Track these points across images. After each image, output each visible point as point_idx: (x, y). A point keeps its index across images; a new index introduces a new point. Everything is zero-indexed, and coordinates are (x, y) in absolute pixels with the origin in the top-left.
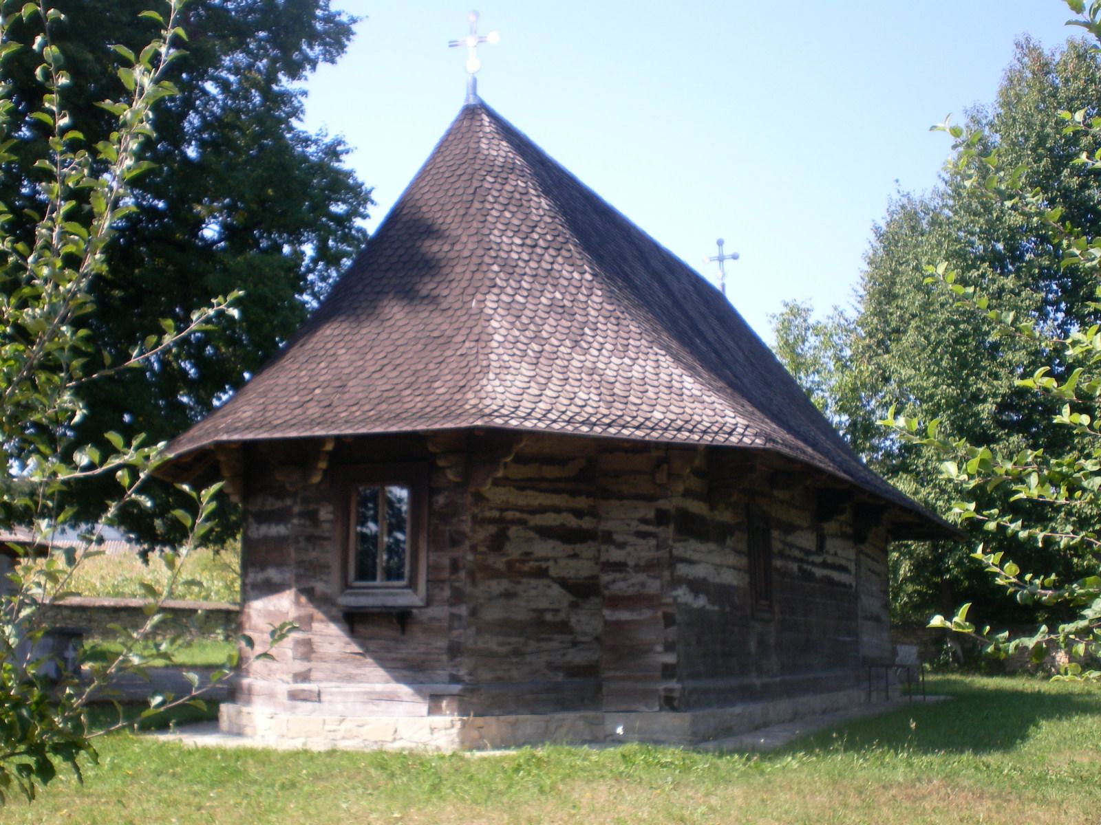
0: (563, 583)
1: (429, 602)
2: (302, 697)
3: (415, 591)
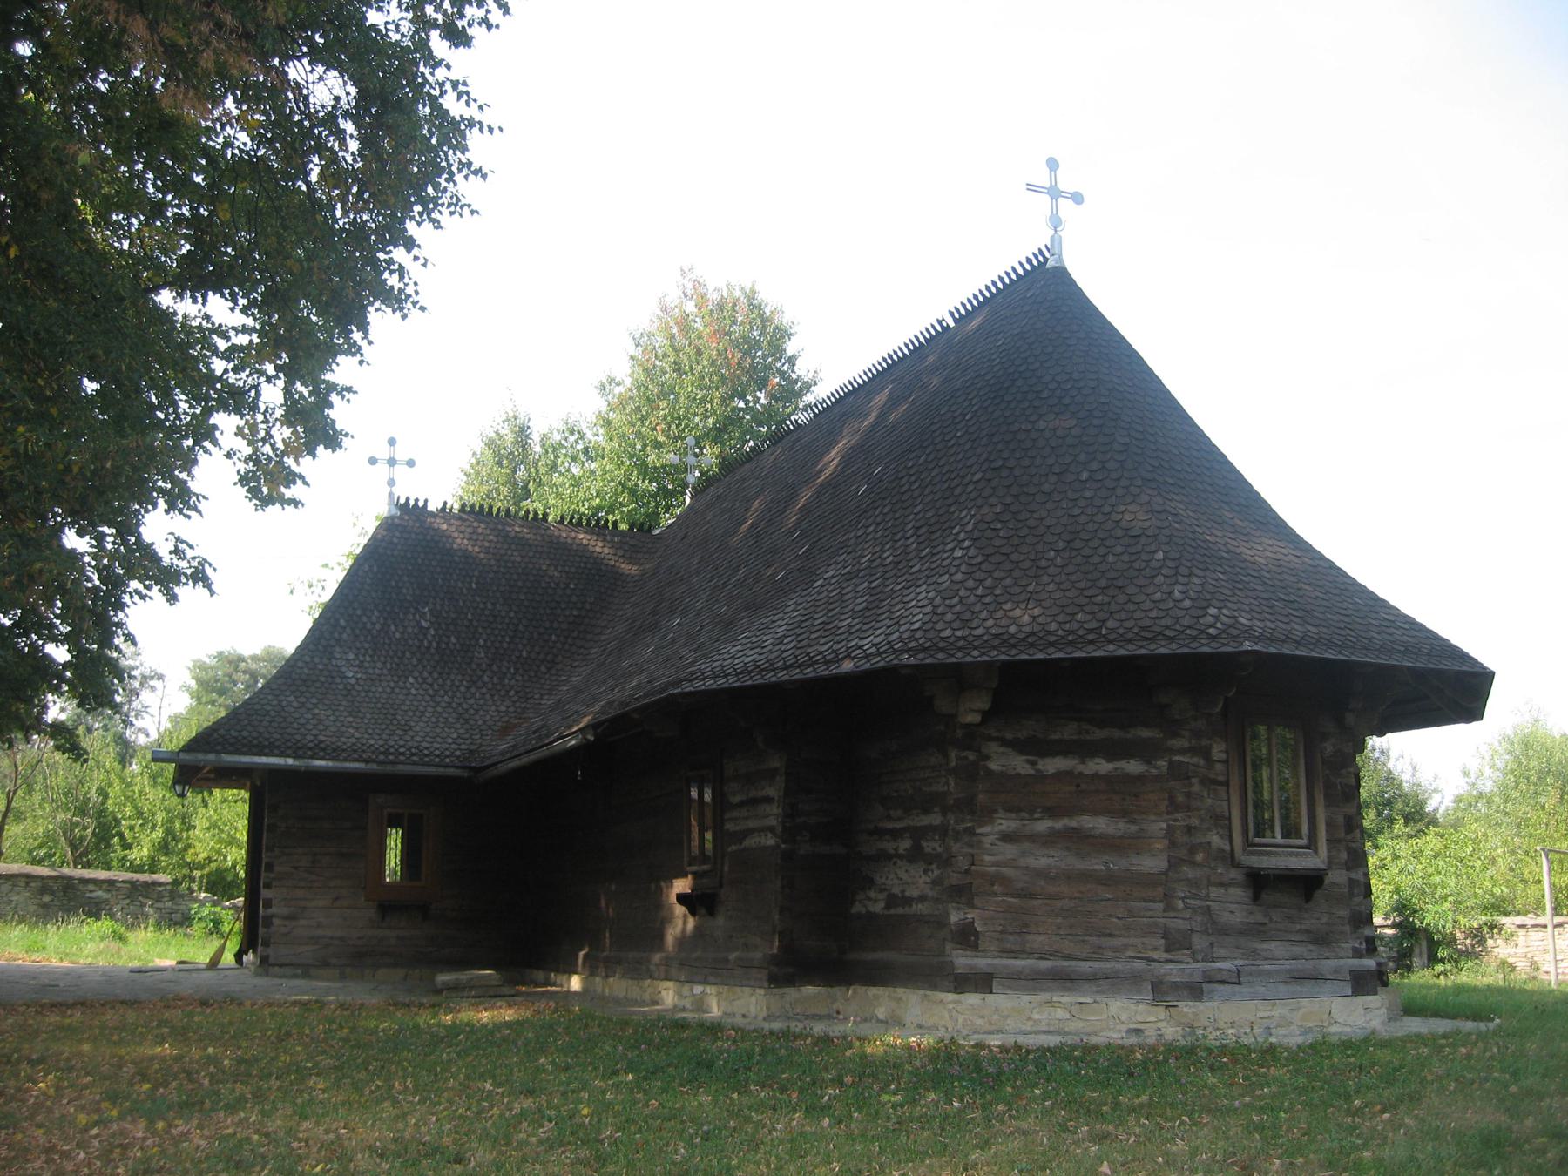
2: (1219, 977)
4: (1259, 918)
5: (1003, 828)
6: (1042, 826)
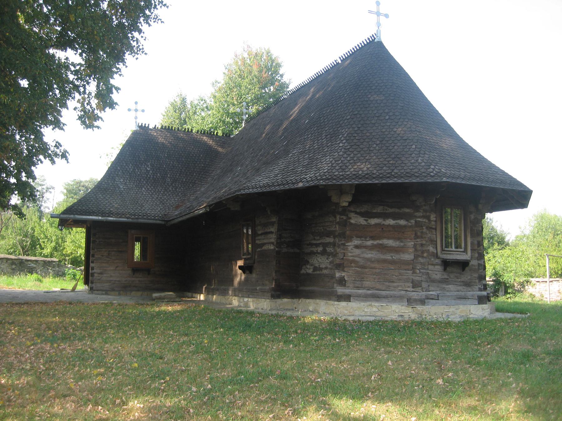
2: (431, 297)
4: (446, 277)
5: (355, 243)
6: (369, 243)
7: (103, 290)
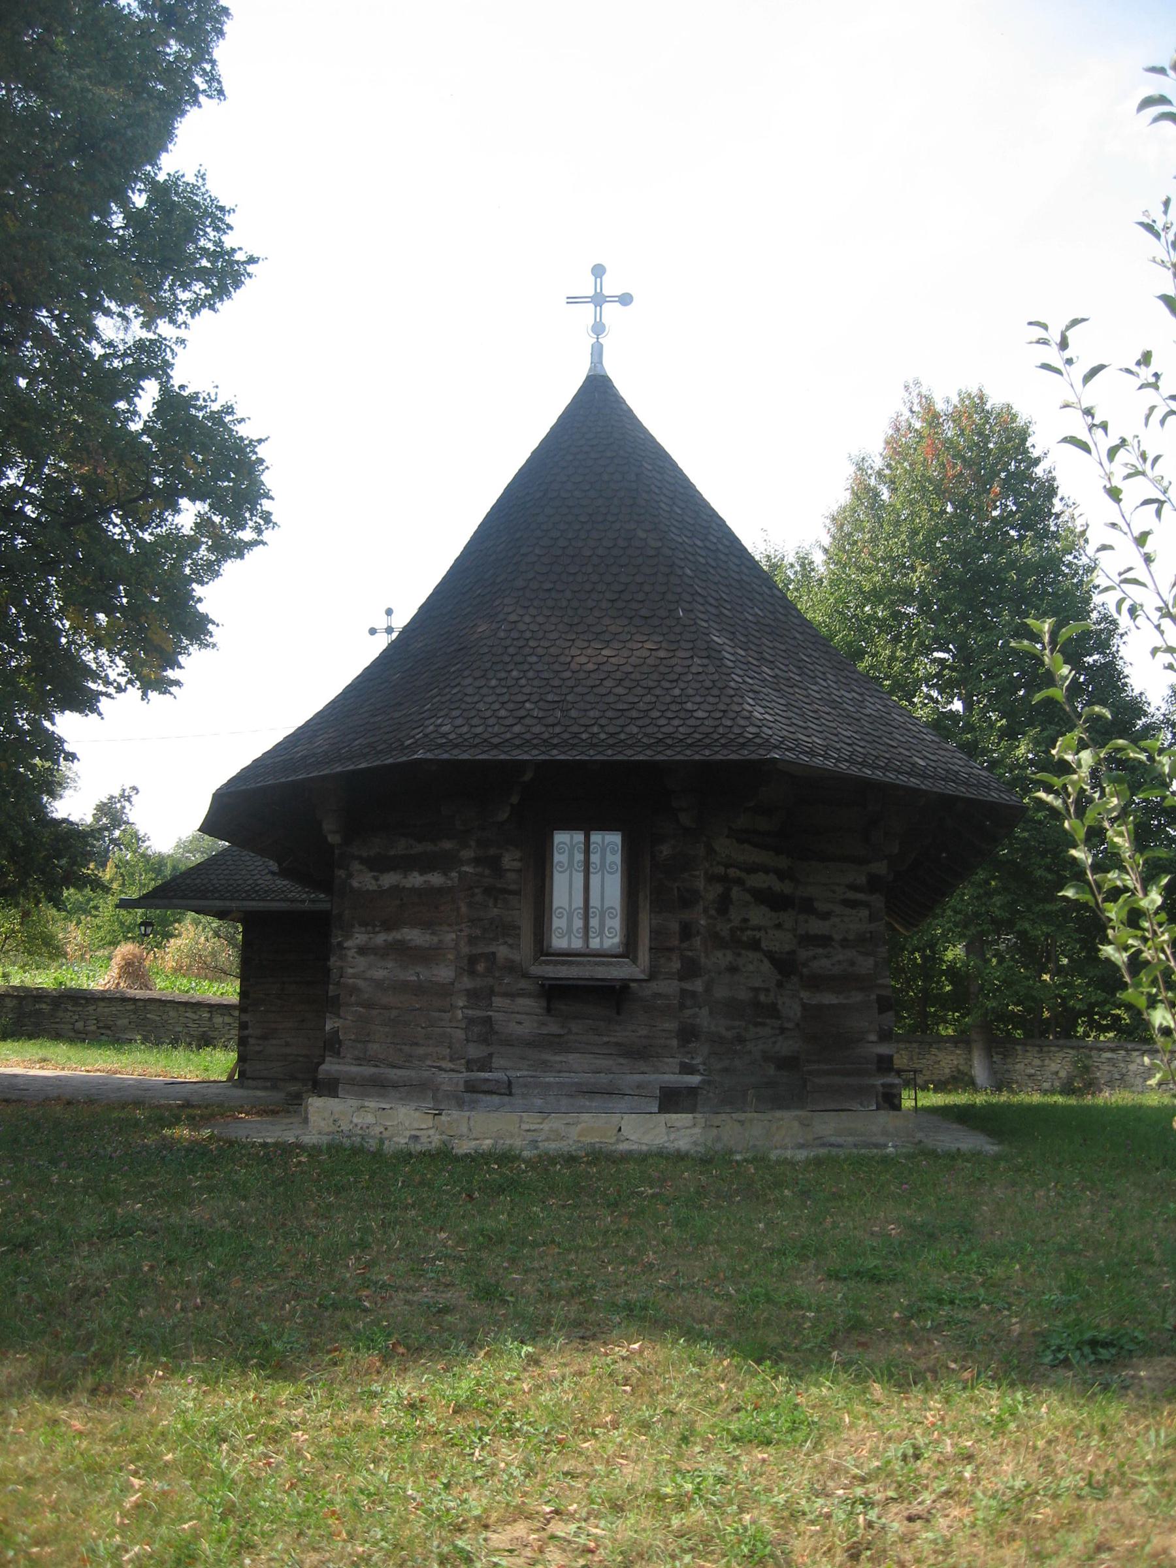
0: (771, 957)
1: (653, 976)
2: (485, 1088)
3: (634, 961)
4: (554, 1028)
5: (358, 941)
6: (381, 939)
7: (265, 1079)
